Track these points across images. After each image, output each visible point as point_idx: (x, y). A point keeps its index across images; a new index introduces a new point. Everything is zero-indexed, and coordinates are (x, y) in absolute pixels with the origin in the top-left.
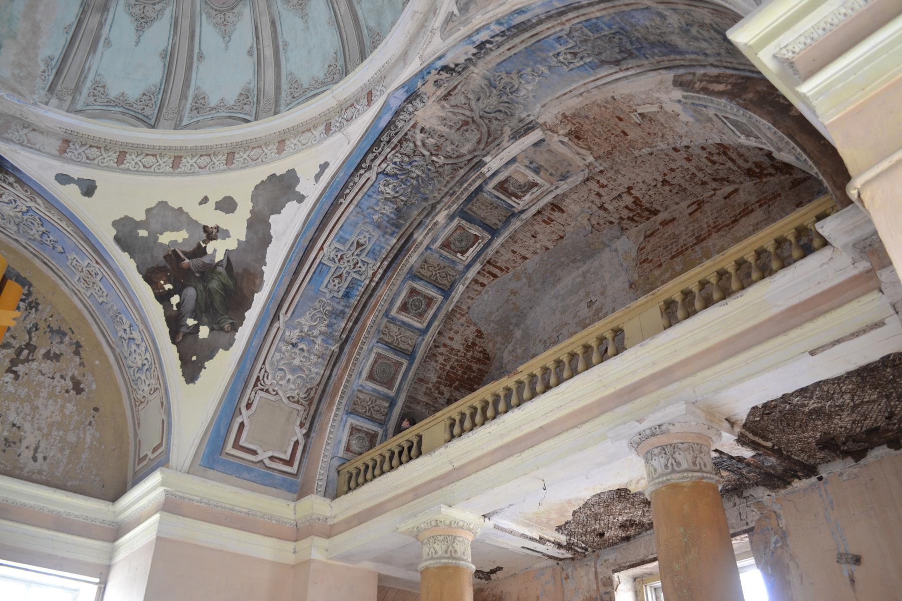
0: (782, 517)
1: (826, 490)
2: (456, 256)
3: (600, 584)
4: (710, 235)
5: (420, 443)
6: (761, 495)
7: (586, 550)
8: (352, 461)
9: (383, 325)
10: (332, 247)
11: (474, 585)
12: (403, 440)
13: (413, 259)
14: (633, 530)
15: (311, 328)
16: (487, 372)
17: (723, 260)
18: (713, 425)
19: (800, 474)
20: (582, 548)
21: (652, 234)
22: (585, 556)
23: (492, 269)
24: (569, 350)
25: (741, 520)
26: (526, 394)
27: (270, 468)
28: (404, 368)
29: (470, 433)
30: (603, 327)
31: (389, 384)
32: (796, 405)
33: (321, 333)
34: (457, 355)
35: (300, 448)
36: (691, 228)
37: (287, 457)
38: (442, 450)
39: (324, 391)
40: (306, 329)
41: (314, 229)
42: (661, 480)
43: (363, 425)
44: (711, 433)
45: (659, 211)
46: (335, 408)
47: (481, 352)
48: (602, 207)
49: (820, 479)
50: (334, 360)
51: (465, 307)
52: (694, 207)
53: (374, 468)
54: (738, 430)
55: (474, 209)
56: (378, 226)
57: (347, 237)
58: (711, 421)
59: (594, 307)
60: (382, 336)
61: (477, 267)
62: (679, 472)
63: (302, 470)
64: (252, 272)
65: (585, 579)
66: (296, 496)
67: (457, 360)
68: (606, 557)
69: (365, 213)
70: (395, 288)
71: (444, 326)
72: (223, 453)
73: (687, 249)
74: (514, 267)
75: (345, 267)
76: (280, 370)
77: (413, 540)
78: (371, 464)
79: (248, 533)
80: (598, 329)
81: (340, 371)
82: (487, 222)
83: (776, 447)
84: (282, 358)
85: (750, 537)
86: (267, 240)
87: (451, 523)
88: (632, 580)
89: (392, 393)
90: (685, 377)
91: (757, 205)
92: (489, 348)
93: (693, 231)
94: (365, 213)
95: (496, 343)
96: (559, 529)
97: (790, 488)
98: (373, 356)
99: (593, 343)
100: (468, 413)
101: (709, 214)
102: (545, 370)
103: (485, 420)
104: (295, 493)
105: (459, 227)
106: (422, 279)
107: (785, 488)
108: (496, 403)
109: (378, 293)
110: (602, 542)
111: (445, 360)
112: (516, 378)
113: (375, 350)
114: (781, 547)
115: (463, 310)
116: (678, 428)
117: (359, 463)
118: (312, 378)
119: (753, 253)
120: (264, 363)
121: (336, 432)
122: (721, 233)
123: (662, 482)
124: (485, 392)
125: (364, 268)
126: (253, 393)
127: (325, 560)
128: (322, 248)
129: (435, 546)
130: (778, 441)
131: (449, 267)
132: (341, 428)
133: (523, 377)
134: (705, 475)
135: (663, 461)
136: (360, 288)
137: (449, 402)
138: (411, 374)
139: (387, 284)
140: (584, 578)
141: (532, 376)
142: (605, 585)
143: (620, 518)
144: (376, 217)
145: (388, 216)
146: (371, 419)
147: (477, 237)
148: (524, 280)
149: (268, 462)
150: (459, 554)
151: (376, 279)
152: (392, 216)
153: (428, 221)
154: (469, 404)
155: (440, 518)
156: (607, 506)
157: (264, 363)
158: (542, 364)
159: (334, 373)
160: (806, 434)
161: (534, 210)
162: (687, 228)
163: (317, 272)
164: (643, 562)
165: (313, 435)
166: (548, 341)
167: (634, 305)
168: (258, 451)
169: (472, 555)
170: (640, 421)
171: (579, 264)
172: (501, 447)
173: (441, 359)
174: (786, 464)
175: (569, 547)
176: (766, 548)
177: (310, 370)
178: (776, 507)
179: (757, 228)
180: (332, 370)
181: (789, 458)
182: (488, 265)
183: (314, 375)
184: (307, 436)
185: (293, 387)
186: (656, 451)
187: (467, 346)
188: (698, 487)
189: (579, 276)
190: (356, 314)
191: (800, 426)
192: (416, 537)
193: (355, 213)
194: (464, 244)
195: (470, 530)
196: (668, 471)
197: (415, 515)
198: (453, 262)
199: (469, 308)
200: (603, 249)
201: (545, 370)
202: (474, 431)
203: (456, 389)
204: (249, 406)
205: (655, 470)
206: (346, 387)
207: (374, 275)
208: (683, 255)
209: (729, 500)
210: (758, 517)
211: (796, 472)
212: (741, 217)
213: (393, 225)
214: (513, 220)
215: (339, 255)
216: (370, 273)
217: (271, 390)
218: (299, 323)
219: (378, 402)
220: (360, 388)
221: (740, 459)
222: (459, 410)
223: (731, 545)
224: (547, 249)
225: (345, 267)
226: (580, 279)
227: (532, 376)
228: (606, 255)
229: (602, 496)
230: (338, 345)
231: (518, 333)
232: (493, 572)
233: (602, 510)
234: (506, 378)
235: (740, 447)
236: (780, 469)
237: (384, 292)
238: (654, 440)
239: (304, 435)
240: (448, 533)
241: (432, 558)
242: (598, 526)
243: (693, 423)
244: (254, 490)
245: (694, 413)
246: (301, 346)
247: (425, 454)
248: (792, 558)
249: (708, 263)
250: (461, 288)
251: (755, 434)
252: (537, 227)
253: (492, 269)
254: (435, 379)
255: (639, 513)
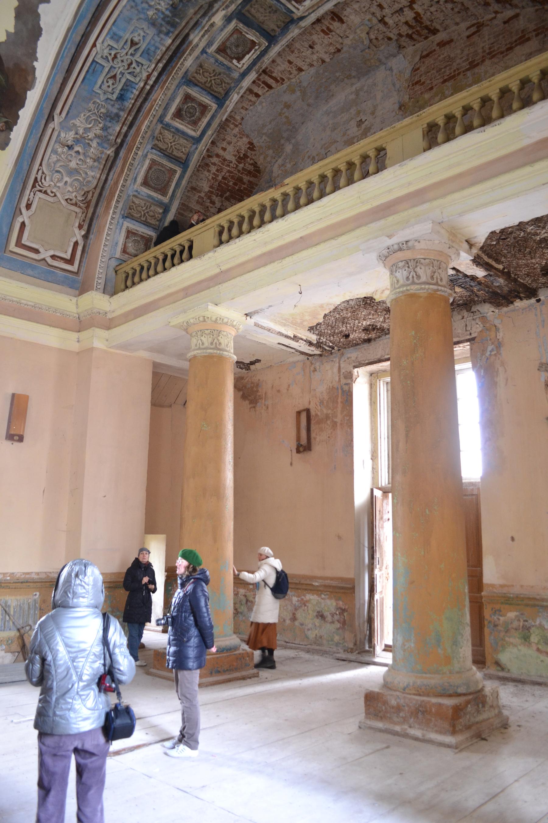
0: (501, 330)
1: (541, 311)
2: (231, 62)
3: (342, 376)
4: (483, 61)
5: (191, 248)
6: (486, 311)
7: (333, 348)
8: (129, 262)
9: (157, 131)
10: (106, 44)
11: (235, 374)
12: (174, 244)
13: (188, 62)
14: (374, 333)
15: (86, 130)
16: (257, 185)
17: (487, 87)
18: (454, 245)
19: (522, 295)
20: (330, 347)
21: (428, 55)
22: (331, 354)
23: (267, 78)
24: (333, 166)
25: (466, 330)
26: (290, 206)
27: (52, 266)
28: (177, 176)
29: (237, 240)
30: (366, 146)
31: (163, 191)
32: (530, 233)
33: (97, 136)
34: (229, 166)
35: (80, 248)
36: (466, 52)
37: (68, 256)
38: (211, 254)
39: (100, 195)
40: (81, 131)
41: (86, 22)
42: (401, 289)
43: (138, 229)
44: (451, 252)
45: (438, 31)
46: (111, 212)
47: (251, 164)
48: (382, 21)
49: (538, 301)
50: (110, 164)
51: (238, 118)
52: (473, 29)
53: (148, 269)
54: (475, 251)
55: (253, 11)
56: (153, 23)
57: (121, 33)
58: (453, 242)
59: (363, 126)
60: (157, 141)
61: (253, 76)
62: (418, 284)
63: (82, 269)
64: (24, 67)
65: (330, 372)
66: (77, 292)
67: (229, 171)
68: (349, 355)
69: (139, 8)
70: (169, 93)
71: (218, 136)
72: (7, 251)
73: (459, 74)
74: (289, 79)
75: (120, 67)
76: (58, 172)
77: (184, 333)
78: (146, 265)
79: (35, 324)
80: (362, 147)
81: (116, 176)
82: (265, 27)
83: (506, 270)
84: (58, 160)
85: (471, 345)
86: (36, 32)
87: (216, 319)
88: (369, 375)
89: (166, 200)
90: (435, 199)
91: (534, 33)
92: (260, 161)
93: (468, 55)
94: (139, 8)
95: (267, 156)
96: (311, 329)
97: (511, 307)
98: (147, 162)
99: (357, 160)
100: (236, 221)
101: (487, 37)
102: (310, 184)
103: (251, 228)
104: (76, 289)
105: (236, 30)
106: (196, 85)
107: (507, 306)
108: (262, 213)
109: (153, 97)
110: (346, 342)
111: (217, 170)
112: (282, 190)
113: (150, 156)
114: (495, 355)
115: (236, 120)
116: (422, 245)
117: (135, 264)
118: (89, 182)
119: (518, 82)
120: (41, 165)
121: (113, 234)
122: (495, 60)
123: (402, 292)
124: (252, 203)
125: (138, 70)
126: (32, 194)
127: (105, 348)
128: (94, 45)
129: (203, 338)
130: (509, 265)
131: (224, 73)
132: (118, 231)
133: (289, 189)
134: (440, 288)
135: (405, 273)
136: (134, 91)
137: (220, 211)
138: (184, 182)
139: (162, 88)
140: (329, 372)
141: (298, 189)
142: (345, 377)
143: (364, 323)
144: (150, 13)
145: (163, 13)
146: (146, 224)
147: (253, 43)
148: (298, 93)
149: (49, 260)
150: (223, 346)
151: (151, 82)
152: (168, 13)
153: (204, 22)
154: (237, 212)
155: (207, 314)
156: (354, 312)
157: (41, 165)
158: (307, 178)
159: (110, 178)
160: (533, 261)
161: (313, 17)
162: (462, 51)
163: (91, 71)
164: (380, 361)
165: (91, 236)
166: (317, 158)
167: (398, 125)
168: (41, 250)
169: (234, 349)
170: (390, 237)
171: (354, 80)
172: (264, 254)
173: (213, 169)
174: (512, 285)
175: (318, 345)
176: (482, 354)
177: (86, 174)
178: (497, 322)
179: (529, 56)
180: (108, 175)
181: (515, 280)
182: (263, 75)
183: (90, 179)
184: (86, 237)
185: (71, 190)
186: (401, 264)
187: (239, 157)
188: (432, 297)
189: (352, 93)
190: (130, 118)
191: (530, 253)
192: (186, 330)
193: (128, 7)
194: (240, 49)
195: (233, 326)
196: (408, 282)
197: (185, 312)
198: (229, 68)
199: (243, 119)
200: (378, 67)
201: (310, 184)
202: (240, 238)
203: (227, 199)
204: (28, 206)
205: (398, 281)
206: (121, 191)
207: (148, 77)
208: (454, 79)
209: (459, 313)
210: (480, 329)
211: (519, 293)
212: (516, 45)
213: (168, 23)
214: (292, 27)
215: (113, 53)
216: (145, 75)
217: (49, 192)
218: (74, 125)
219: (153, 208)
220: (136, 193)
221: (473, 278)
222: (228, 217)
223: (452, 351)
224: (323, 61)
225: (120, 67)
226: (353, 96)
227: (298, 189)
228: (381, 74)
229: (351, 303)
230: (113, 149)
231: (288, 148)
232: (252, 363)
233: (349, 314)
234: (273, 189)
235: (475, 267)
236: (506, 289)
237: (159, 97)
238: (400, 255)
239: (83, 236)
240: (214, 328)
241: (199, 349)
242: (344, 329)
243: (437, 242)
244: (38, 286)
245: (439, 232)
246: (77, 148)
247: (196, 257)
248: (503, 364)
249: (475, 88)
250: (235, 97)
251: (490, 257)
252: (315, 37)
253: (267, 78)
254: (207, 189)
255: (381, 319)
